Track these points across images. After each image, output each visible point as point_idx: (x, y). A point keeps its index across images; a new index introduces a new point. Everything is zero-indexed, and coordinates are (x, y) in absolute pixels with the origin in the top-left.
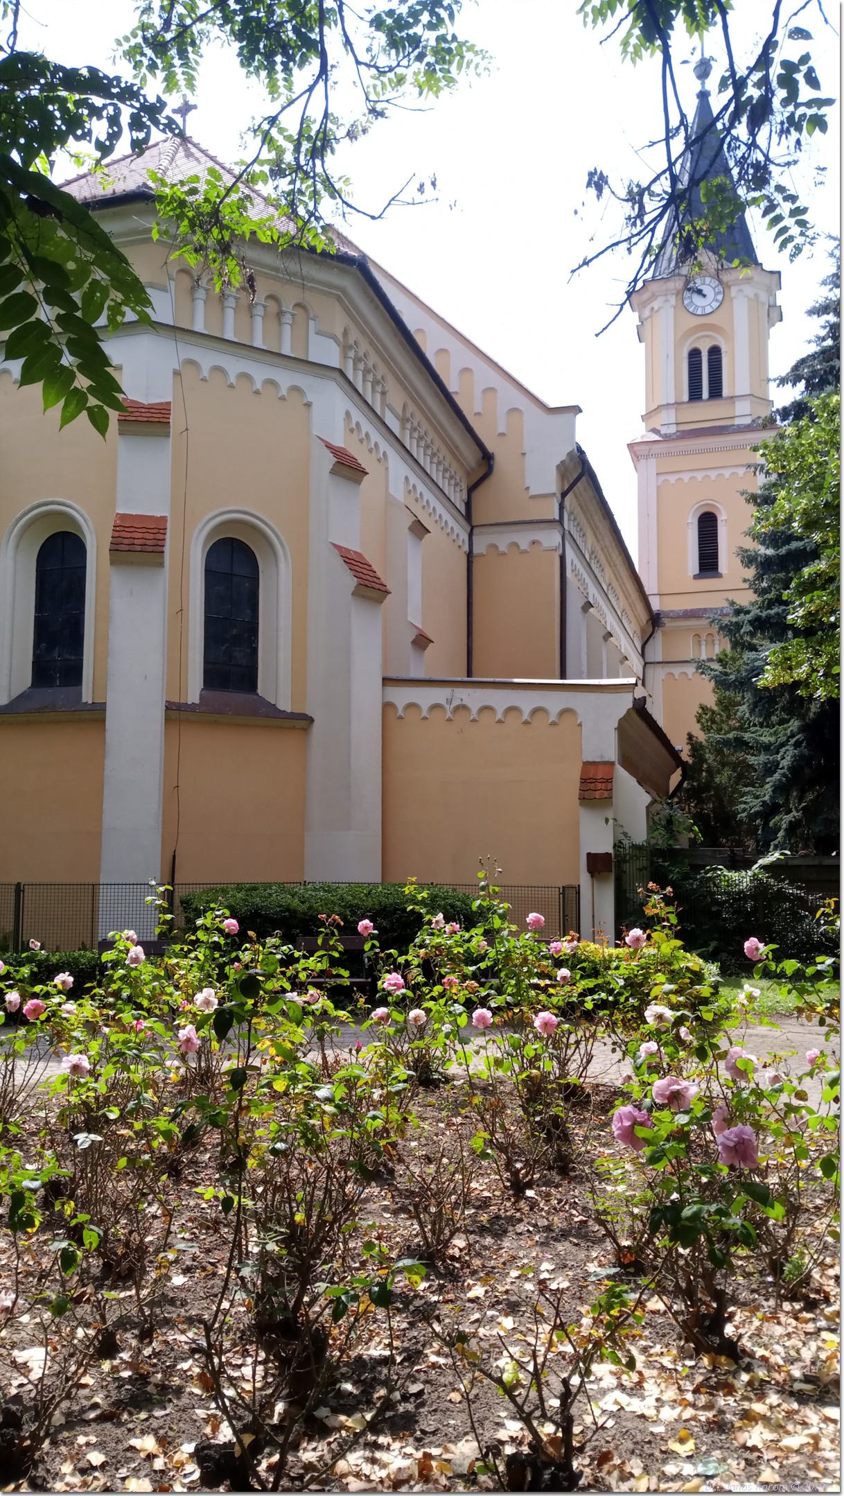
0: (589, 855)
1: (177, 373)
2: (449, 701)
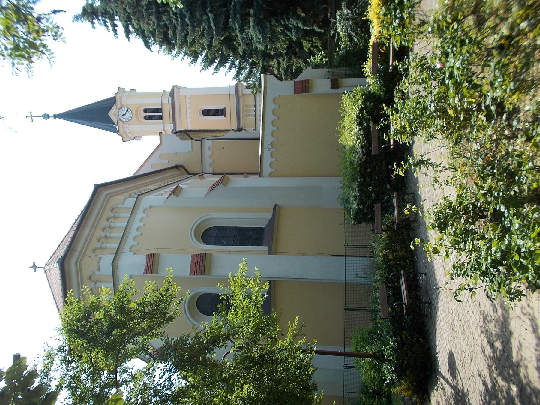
0: (332, 88)
1: (135, 254)
2: (269, 150)
